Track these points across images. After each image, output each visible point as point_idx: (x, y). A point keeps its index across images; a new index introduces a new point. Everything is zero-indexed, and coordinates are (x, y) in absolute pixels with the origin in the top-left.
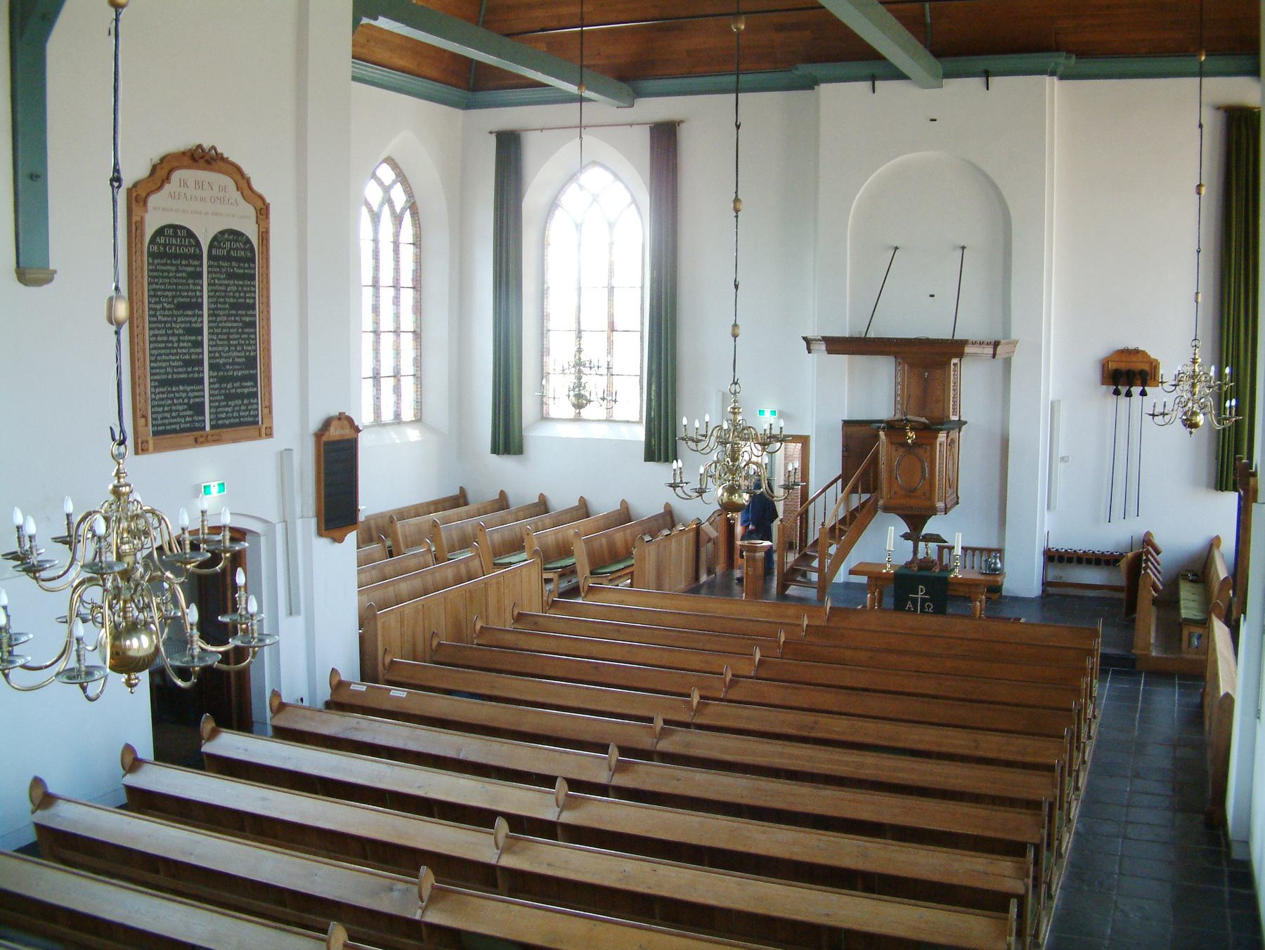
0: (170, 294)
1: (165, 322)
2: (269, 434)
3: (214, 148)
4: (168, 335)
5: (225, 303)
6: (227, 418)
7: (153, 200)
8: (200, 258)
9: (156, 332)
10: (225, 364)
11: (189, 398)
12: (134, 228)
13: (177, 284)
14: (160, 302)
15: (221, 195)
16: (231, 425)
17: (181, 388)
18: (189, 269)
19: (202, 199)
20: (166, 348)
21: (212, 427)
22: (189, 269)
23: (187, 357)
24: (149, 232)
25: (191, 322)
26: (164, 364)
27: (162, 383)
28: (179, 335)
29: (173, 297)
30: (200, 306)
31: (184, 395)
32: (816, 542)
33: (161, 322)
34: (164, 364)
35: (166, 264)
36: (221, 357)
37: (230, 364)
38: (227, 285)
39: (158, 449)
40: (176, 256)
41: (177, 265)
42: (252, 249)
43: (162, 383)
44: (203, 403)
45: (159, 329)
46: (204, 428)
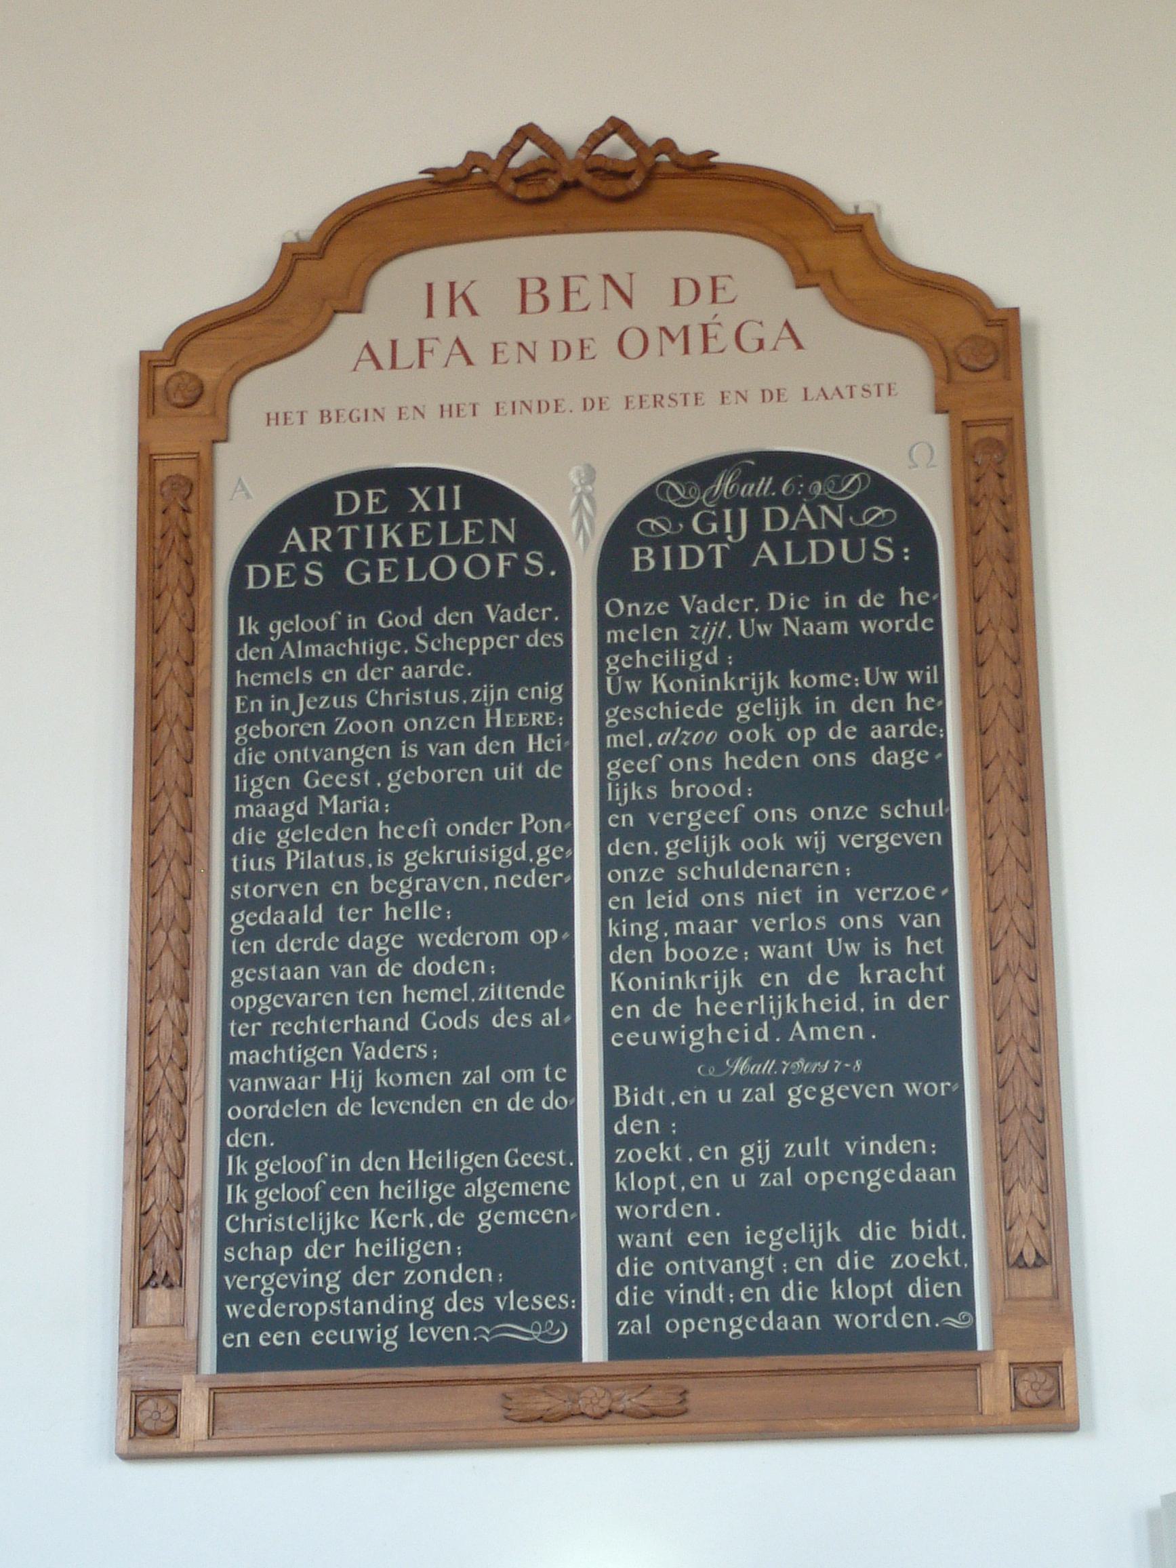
0: (357, 755)
1: (325, 877)
2: (1045, 1400)
3: (616, 126)
4: (345, 930)
5: (720, 775)
6: (725, 1310)
7: (255, 394)
8: (557, 591)
9: (269, 918)
10: (716, 1054)
11: (473, 1207)
12: (170, 506)
13: (400, 713)
14: (297, 792)
15: (696, 314)
16: (755, 1344)
17: (419, 1159)
18: (484, 644)
19: (774, 395)
20: (327, 983)
21: (618, 1347)
22: (484, 644)
23: (464, 1022)
24: (234, 523)
25: (487, 871)
26: (311, 1056)
27: (293, 1138)
28: (411, 929)
29: (379, 769)
30: (558, 799)
31: (435, 1194)
32: (541, 147)
33: (299, 875)
34: (311, 1056)
35: (341, 634)
36: (691, 1020)
37: (757, 1053)
38: (730, 700)
39: (227, 1443)
40: (400, 597)
41: (406, 635)
42: (911, 523)
43: (293, 1138)
44: (572, 1231)
45: (287, 904)
46: (572, 1349)
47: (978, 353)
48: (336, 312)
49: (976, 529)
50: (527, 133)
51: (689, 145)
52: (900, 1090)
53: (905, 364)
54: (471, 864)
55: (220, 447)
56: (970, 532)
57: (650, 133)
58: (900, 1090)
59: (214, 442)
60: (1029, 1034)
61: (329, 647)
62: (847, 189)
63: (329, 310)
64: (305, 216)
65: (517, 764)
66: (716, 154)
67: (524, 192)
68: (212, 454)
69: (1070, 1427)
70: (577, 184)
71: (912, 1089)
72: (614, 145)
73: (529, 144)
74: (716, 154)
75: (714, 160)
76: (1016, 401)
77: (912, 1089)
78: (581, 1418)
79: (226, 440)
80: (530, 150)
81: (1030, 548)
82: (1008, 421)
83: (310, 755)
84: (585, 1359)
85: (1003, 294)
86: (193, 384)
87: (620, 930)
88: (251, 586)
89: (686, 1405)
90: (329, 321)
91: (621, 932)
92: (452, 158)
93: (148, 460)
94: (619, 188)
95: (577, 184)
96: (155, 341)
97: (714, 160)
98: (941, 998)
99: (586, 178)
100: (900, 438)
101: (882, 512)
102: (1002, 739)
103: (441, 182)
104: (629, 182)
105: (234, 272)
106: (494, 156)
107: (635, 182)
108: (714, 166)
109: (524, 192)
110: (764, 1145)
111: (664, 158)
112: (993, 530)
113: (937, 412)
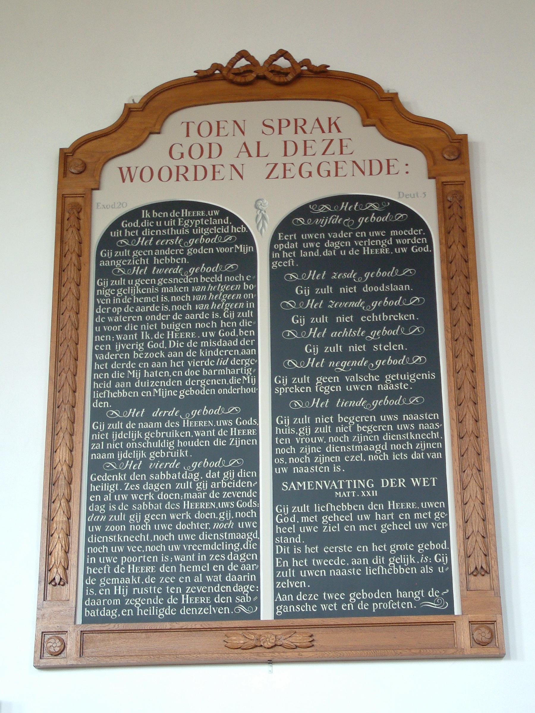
3: (283, 54)
47: (448, 154)
48: (151, 133)
49: (449, 246)
50: (243, 54)
51: (316, 62)
52: (408, 483)
53: (415, 160)
54: (288, 434)
55: (96, 193)
56: (446, 233)
57: (298, 58)
58: (408, 483)
59: (93, 189)
60: (468, 333)
61: (133, 274)
62: (388, 85)
63: (148, 132)
64: (137, 93)
65: (119, 231)
66: (329, 66)
67: (239, 79)
68: (91, 194)
69: (499, 656)
70: (264, 78)
71: (416, 482)
72: (282, 63)
73: (243, 59)
74: (329, 66)
75: (328, 69)
76: (467, 172)
77: (416, 482)
78: (261, 648)
79: (98, 189)
80: (243, 62)
81: (473, 230)
82: (462, 183)
83: (371, 493)
84: (262, 619)
85: (459, 128)
86: (80, 163)
87: (205, 354)
88: (383, 486)
89: (313, 638)
90: (148, 137)
91: (205, 354)
92: (205, 66)
93: (62, 198)
94: (283, 79)
95: (264, 78)
96: (67, 145)
97: (328, 69)
98: (350, 233)
99: (270, 76)
100: (412, 187)
101: (402, 215)
102: (476, 525)
103: (203, 77)
104: (287, 78)
105: (106, 117)
106: (225, 65)
107: (290, 77)
108: (328, 71)
109: (239, 79)
110: (232, 472)
111: (305, 68)
112: (461, 292)
113: (429, 178)
